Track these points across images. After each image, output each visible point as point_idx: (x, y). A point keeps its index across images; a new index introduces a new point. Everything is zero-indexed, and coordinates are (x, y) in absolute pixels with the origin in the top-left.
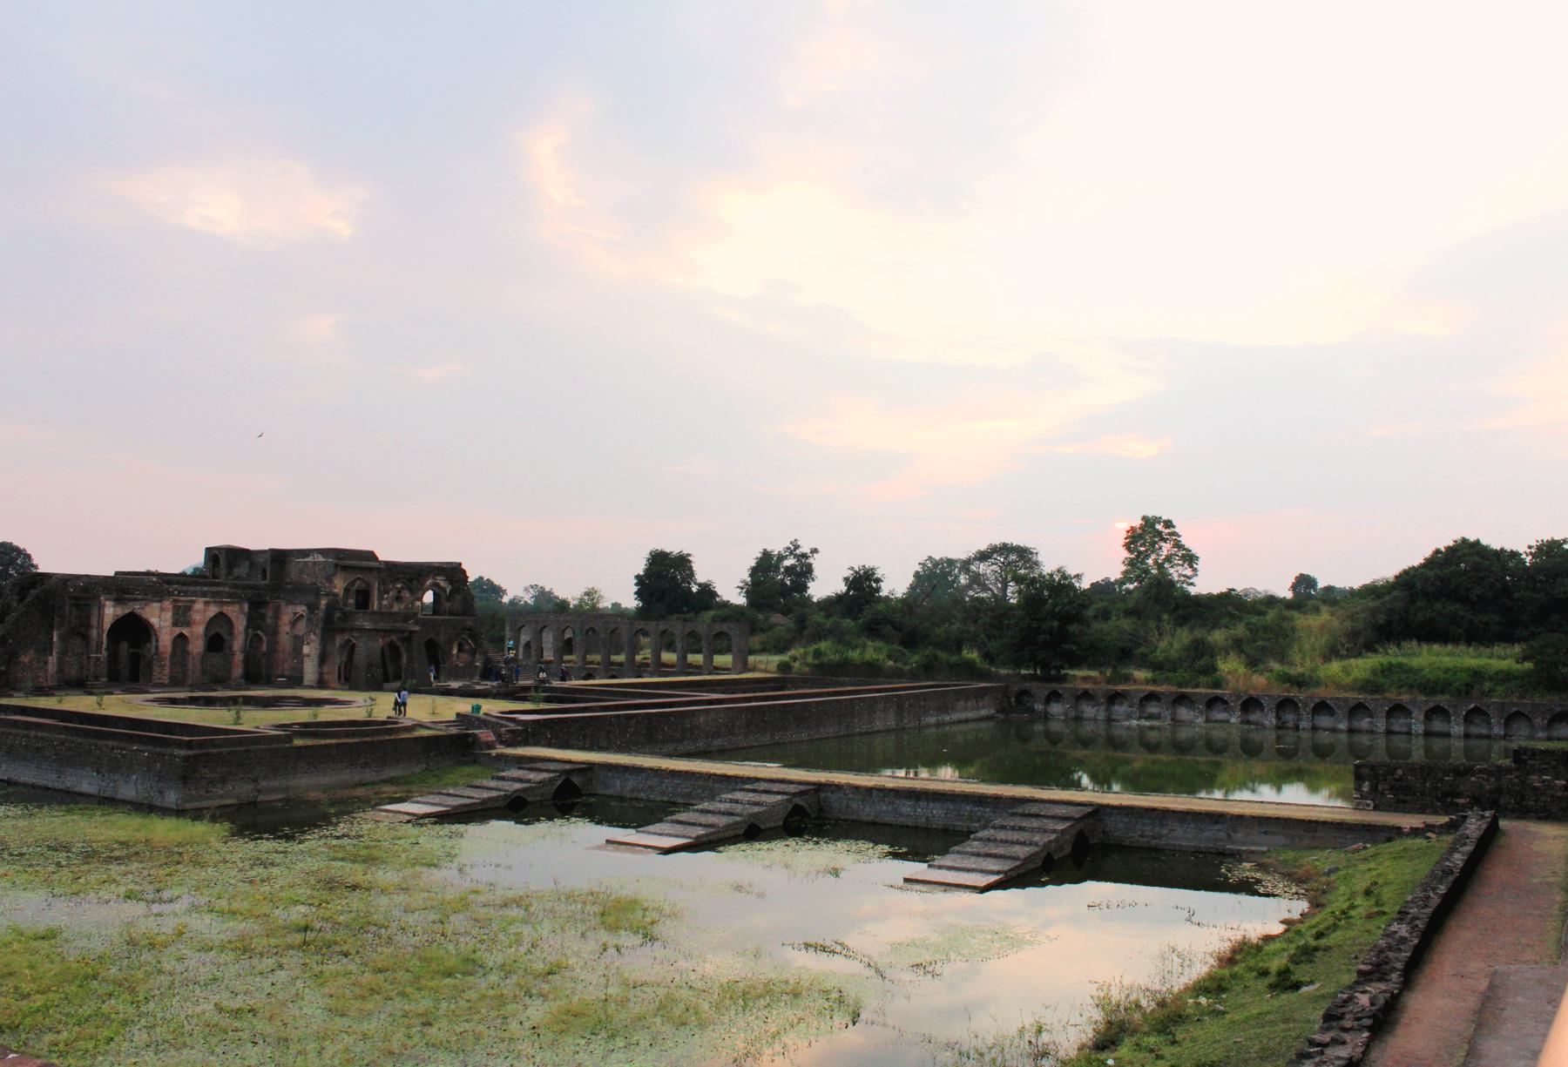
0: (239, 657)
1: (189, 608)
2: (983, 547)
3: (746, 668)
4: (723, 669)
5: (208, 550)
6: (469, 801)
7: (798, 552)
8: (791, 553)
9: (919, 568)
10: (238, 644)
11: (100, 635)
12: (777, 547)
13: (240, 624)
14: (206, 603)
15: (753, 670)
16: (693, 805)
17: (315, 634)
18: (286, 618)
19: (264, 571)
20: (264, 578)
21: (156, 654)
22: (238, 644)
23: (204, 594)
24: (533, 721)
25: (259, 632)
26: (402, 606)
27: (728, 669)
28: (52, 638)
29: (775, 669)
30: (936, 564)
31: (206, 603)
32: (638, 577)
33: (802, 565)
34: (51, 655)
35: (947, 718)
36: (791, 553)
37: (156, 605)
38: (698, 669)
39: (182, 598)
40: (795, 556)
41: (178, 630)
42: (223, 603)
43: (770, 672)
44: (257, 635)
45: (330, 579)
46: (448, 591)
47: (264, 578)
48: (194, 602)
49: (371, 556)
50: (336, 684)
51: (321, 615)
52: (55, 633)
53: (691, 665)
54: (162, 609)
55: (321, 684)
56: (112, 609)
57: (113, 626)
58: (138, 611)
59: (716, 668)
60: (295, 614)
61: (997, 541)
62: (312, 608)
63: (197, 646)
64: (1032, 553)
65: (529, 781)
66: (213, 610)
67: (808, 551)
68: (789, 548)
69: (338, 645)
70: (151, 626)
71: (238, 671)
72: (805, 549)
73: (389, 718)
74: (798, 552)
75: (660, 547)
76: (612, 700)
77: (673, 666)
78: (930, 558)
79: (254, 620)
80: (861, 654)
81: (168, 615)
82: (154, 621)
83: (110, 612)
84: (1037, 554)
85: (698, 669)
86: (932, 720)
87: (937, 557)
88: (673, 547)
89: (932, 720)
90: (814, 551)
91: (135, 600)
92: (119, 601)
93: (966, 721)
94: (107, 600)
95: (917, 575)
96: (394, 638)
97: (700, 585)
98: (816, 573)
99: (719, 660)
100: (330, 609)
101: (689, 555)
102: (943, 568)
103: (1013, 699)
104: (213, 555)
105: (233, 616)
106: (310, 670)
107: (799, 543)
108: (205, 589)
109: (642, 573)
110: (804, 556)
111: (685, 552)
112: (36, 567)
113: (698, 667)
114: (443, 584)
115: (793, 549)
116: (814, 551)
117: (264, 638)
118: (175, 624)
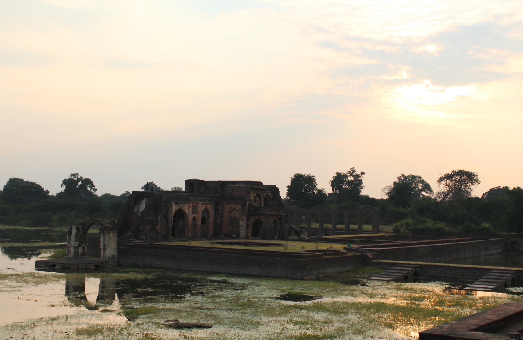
0: (212, 226)
1: (196, 206)
2: (449, 172)
3: (378, 231)
4: (366, 231)
5: (187, 181)
6: (397, 276)
7: (354, 174)
8: (351, 175)
9: (397, 180)
10: (211, 221)
11: (171, 217)
12: (344, 171)
13: (212, 212)
14: (202, 204)
15: (382, 232)
16: (478, 279)
17: (245, 217)
18: (226, 210)
19: (216, 190)
20: (216, 193)
21: (187, 225)
22: (211, 221)
23: (201, 200)
24: (380, 250)
25: (217, 216)
26: (256, 204)
27: (369, 231)
28: (158, 219)
29: (392, 231)
30: (405, 178)
31: (202, 204)
32: (288, 187)
33: (357, 180)
34: (158, 225)
35: (488, 253)
36: (351, 175)
37: (187, 205)
38: (354, 232)
39: (195, 202)
40: (354, 176)
41: (194, 215)
42: (207, 204)
43: (390, 233)
44: (217, 217)
45: (249, 194)
46: (271, 197)
47: (216, 193)
48: (198, 203)
49: (260, 183)
50: (251, 237)
51: (247, 208)
52: (159, 217)
53: (350, 230)
54: (189, 207)
55: (247, 237)
56: (174, 207)
57: (175, 213)
58: (182, 207)
59: (363, 231)
60: (231, 208)
61: (456, 169)
62: (243, 206)
63: (199, 222)
64: (474, 175)
65: (403, 273)
66: (204, 207)
67: (360, 173)
68: (350, 172)
69: (252, 221)
70: (185, 213)
71: (211, 232)
72: (358, 172)
73: (328, 249)
74: (354, 174)
75: (299, 172)
76: (486, 239)
77: (344, 230)
78: (403, 175)
79: (216, 210)
80: (423, 225)
81: (191, 209)
82: (187, 211)
83: (174, 208)
84: (477, 175)
85: (354, 232)
86: (483, 253)
87: (406, 174)
88: (305, 172)
89: (483, 253)
90: (363, 173)
91: (182, 203)
92: (177, 203)
93: (494, 254)
94: (173, 203)
95: (395, 183)
96: (276, 218)
97: (318, 190)
98: (364, 184)
99: (365, 227)
100: (250, 206)
101: (313, 176)
102: (409, 180)
103: (509, 245)
104: (190, 183)
105: (209, 209)
106: (243, 231)
107: (355, 169)
108: (201, 198)
109: (290, 185)
110: (358, 175)
111: (312, 175)
112: (161, 189)
113: (356, 230)
114: (269, 194)
115: (352, 172)
116: (363, 173)
117: (219, 218)
118: (193, 213)
